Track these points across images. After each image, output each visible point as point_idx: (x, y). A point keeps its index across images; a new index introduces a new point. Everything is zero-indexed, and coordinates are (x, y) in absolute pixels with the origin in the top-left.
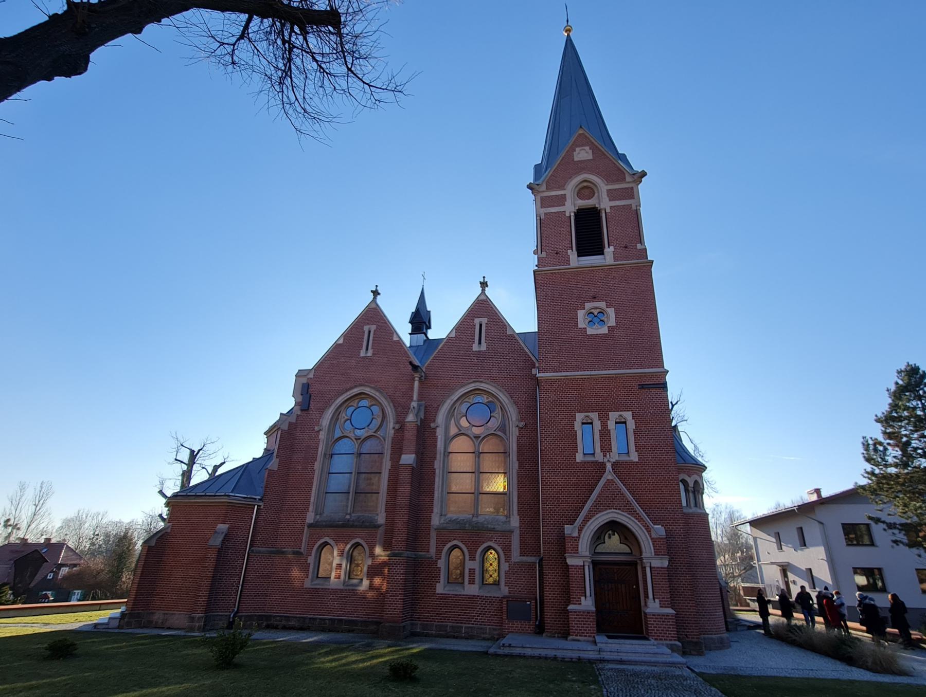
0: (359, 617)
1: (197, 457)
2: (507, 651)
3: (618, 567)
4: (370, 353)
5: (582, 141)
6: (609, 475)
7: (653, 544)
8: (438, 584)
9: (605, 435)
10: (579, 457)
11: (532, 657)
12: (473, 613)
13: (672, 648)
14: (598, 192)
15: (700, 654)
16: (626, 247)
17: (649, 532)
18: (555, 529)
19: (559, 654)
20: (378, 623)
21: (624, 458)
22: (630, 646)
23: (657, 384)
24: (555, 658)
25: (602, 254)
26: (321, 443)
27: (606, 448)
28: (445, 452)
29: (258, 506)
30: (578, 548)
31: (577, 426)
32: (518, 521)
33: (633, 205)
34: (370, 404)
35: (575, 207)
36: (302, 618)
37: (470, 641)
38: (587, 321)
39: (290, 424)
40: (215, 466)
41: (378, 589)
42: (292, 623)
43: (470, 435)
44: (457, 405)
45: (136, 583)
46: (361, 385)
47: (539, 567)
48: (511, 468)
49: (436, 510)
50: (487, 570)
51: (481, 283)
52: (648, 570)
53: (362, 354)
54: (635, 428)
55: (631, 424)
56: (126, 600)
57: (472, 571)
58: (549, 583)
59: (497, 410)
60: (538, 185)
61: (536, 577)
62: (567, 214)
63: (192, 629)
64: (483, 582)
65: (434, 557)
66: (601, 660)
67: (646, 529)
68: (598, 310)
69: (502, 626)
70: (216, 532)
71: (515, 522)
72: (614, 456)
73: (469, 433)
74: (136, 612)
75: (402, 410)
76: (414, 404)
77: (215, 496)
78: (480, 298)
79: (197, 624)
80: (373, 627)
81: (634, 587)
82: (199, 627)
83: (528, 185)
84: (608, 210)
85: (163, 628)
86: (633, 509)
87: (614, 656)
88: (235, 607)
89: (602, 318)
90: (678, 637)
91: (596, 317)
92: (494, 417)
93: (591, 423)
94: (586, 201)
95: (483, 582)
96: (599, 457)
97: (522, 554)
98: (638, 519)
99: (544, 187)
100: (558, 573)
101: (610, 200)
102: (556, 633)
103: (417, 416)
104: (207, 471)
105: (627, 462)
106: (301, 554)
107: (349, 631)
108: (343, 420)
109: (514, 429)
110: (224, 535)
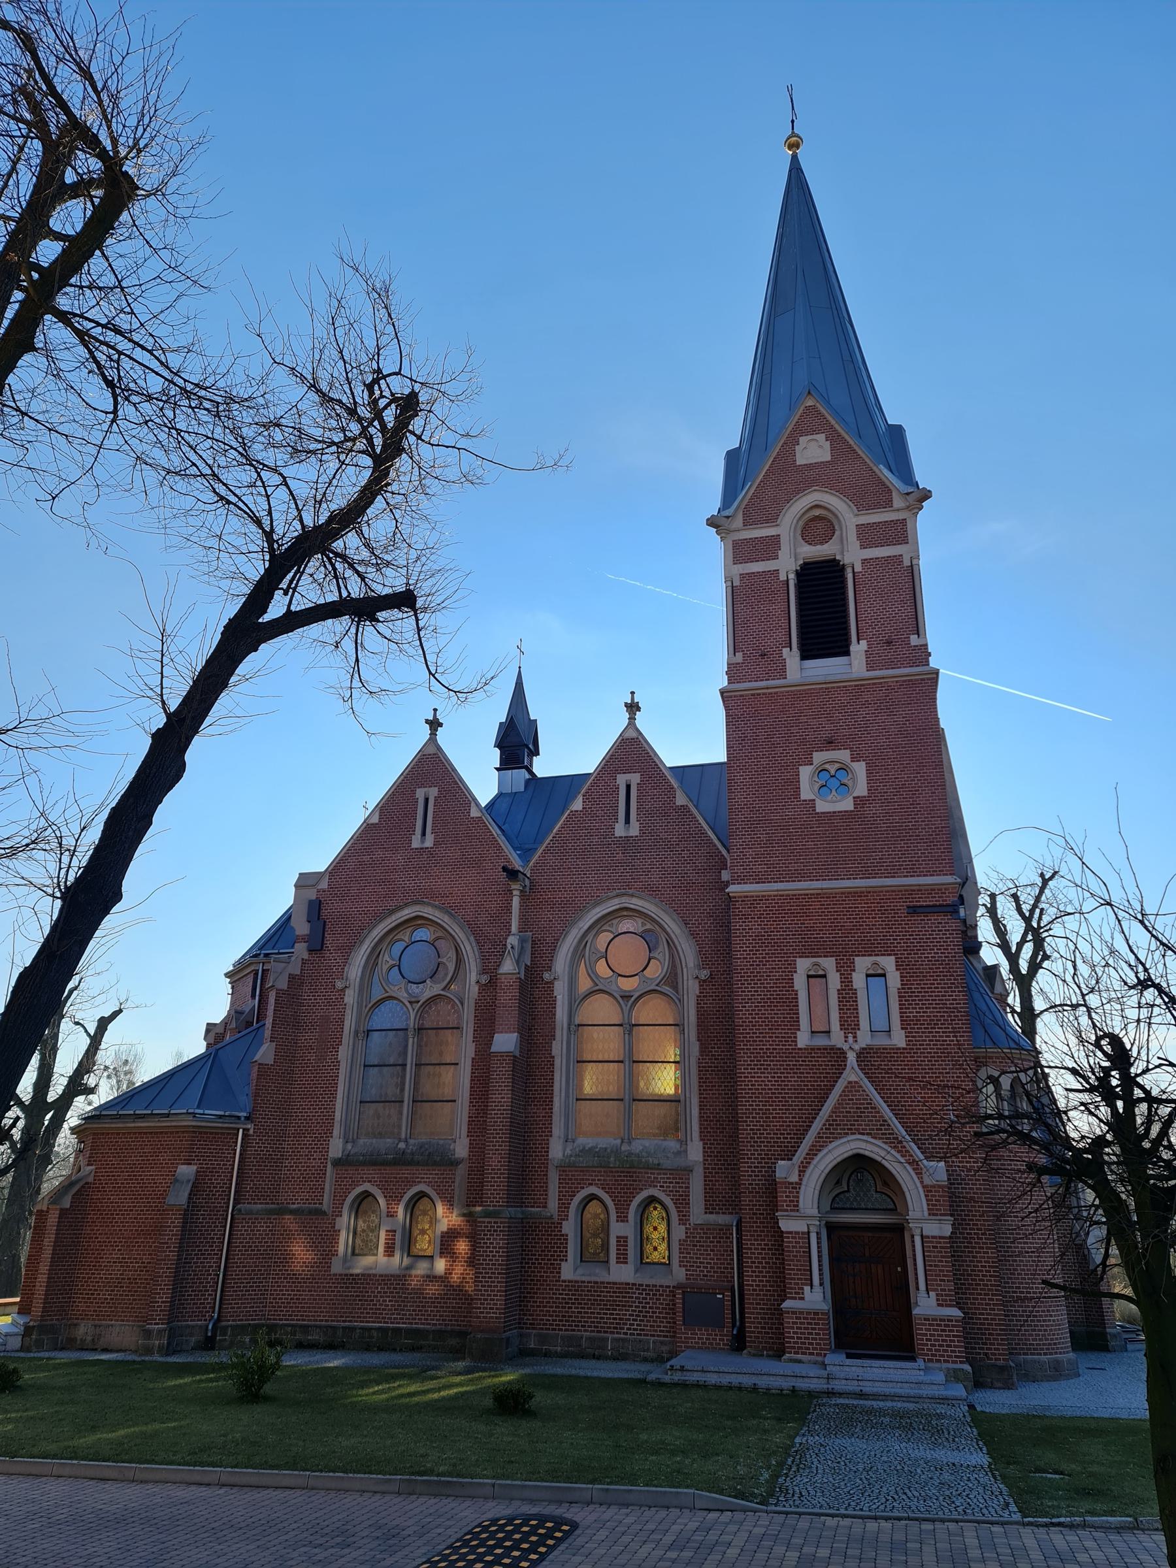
0: (429, 1324)
1: (68, 1004)
2: (677, 1377)
3: (870, 1234)
4: (429, 842)
5: (811, 423)
6: (852, 1073)
7: (926, 1196)
8: (563, 1263)
9: (848, 996)
10: (803, 1039)
11: (718, 1387)
12: (626, 1315)
13: (955, 1376)
14: (841, 529)
15: (1008, 1386)
16: (889, 643)
17: (919, 1174)
18: (762, 1167)
19: (763, 1382)
20: (463, 1334)
21: (881, 1041)
22: (881, 1371)
23: (941, 906)
24: (755, 1389)
25: (847, 653)
26: (348, 1012)
27: (850, 1025)
28: (569, 1025)
29: (244, 1130)
30: (798, 1201)
31: (800, 982)
32: (701, 1149)
33: (904, 556)
34: (434, 937)
35: (796, 560)
36: (331, 1327)
37: (619, 1363)
38: (817, 786)
39: (292, 977)
40: (102, 1019)
41: (443, 1279)
42: (313, 1337)
43: (615, 994)
44: (590, 937)
45: (45, 1274)
46: (416, 902)
47: (737, 1234)
48: (687, 1055)
49: (557, 1130)
50: (648, 1238)
51: (626, 705)
52: (918, 1240)
53: (416, 843)
54: (900, 987)
55: (894, 979)
56: (18, 1299)
57: (622, 1241)
58: (752, 1262)
59: (661, 946)
60: (728, 517)
61: (732, 1251)
62: (783, 577)
63: (148, 1351)
64: (642, 1259)
65: (556, 1217)
66: (828, 1393)
67: (914, 1169)
68: (837, 766)
69: (674, 1337)
70: (176, 1180)
71: (695, 1152)
72: (864, 1039)
73: (612, 988)
74: (49, 1323)
75: (492, 953)
76: (512, 940)
77: (168, 1115)
78: (627, 735)
79: (157, 1342)
80: (453, 1342)
81: (899, 1269)
82: (160, 1348)
83: (708, 520)
84: (858, 568)
85: (96, 1349)
86: (893, 1134)
87: (852, 1387)
88: (213, 1312)
89: (845, 781)
90: (966, 1358)
91: (832, 779)
92: (655, 958)
93: (824, 976)
94: (819, 547)
95: (642, 1259)
96: (837, 1038)
97: (709, 1210)
98: (902, 1151)
99: (738, 522)
100: (768, 1245)
101: (863, 547)
102: (764, 1348)
103: (518, 962)
104: (86, 1031)
105: (886, 1049)
106: (324, 1213)
107: (413, 1349)
108: (385, 967)
109: (691, 982)
110: (190, 1184)
